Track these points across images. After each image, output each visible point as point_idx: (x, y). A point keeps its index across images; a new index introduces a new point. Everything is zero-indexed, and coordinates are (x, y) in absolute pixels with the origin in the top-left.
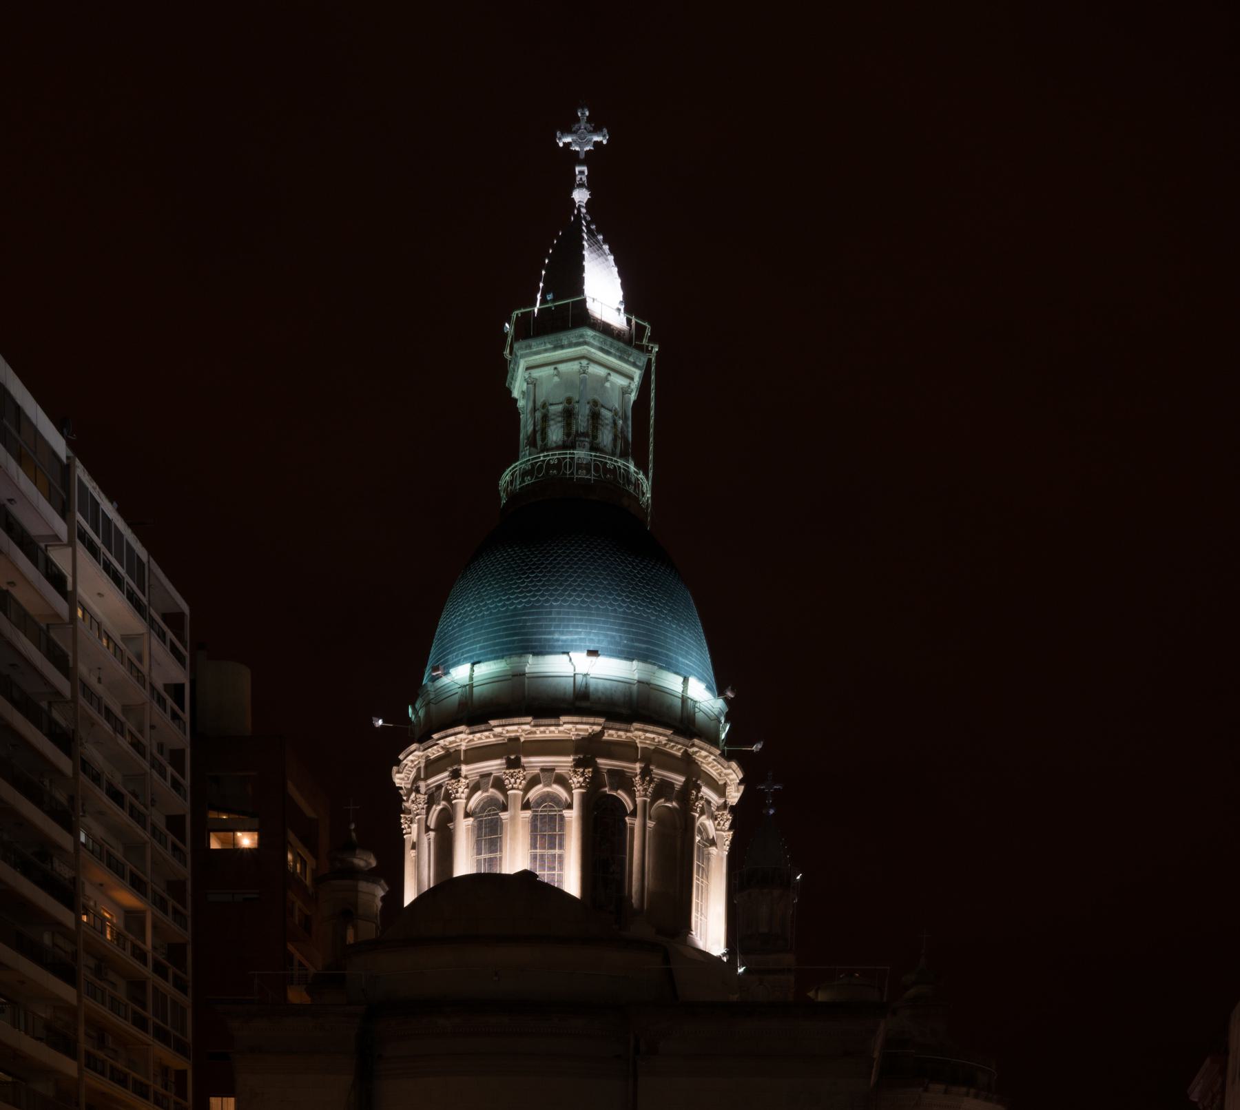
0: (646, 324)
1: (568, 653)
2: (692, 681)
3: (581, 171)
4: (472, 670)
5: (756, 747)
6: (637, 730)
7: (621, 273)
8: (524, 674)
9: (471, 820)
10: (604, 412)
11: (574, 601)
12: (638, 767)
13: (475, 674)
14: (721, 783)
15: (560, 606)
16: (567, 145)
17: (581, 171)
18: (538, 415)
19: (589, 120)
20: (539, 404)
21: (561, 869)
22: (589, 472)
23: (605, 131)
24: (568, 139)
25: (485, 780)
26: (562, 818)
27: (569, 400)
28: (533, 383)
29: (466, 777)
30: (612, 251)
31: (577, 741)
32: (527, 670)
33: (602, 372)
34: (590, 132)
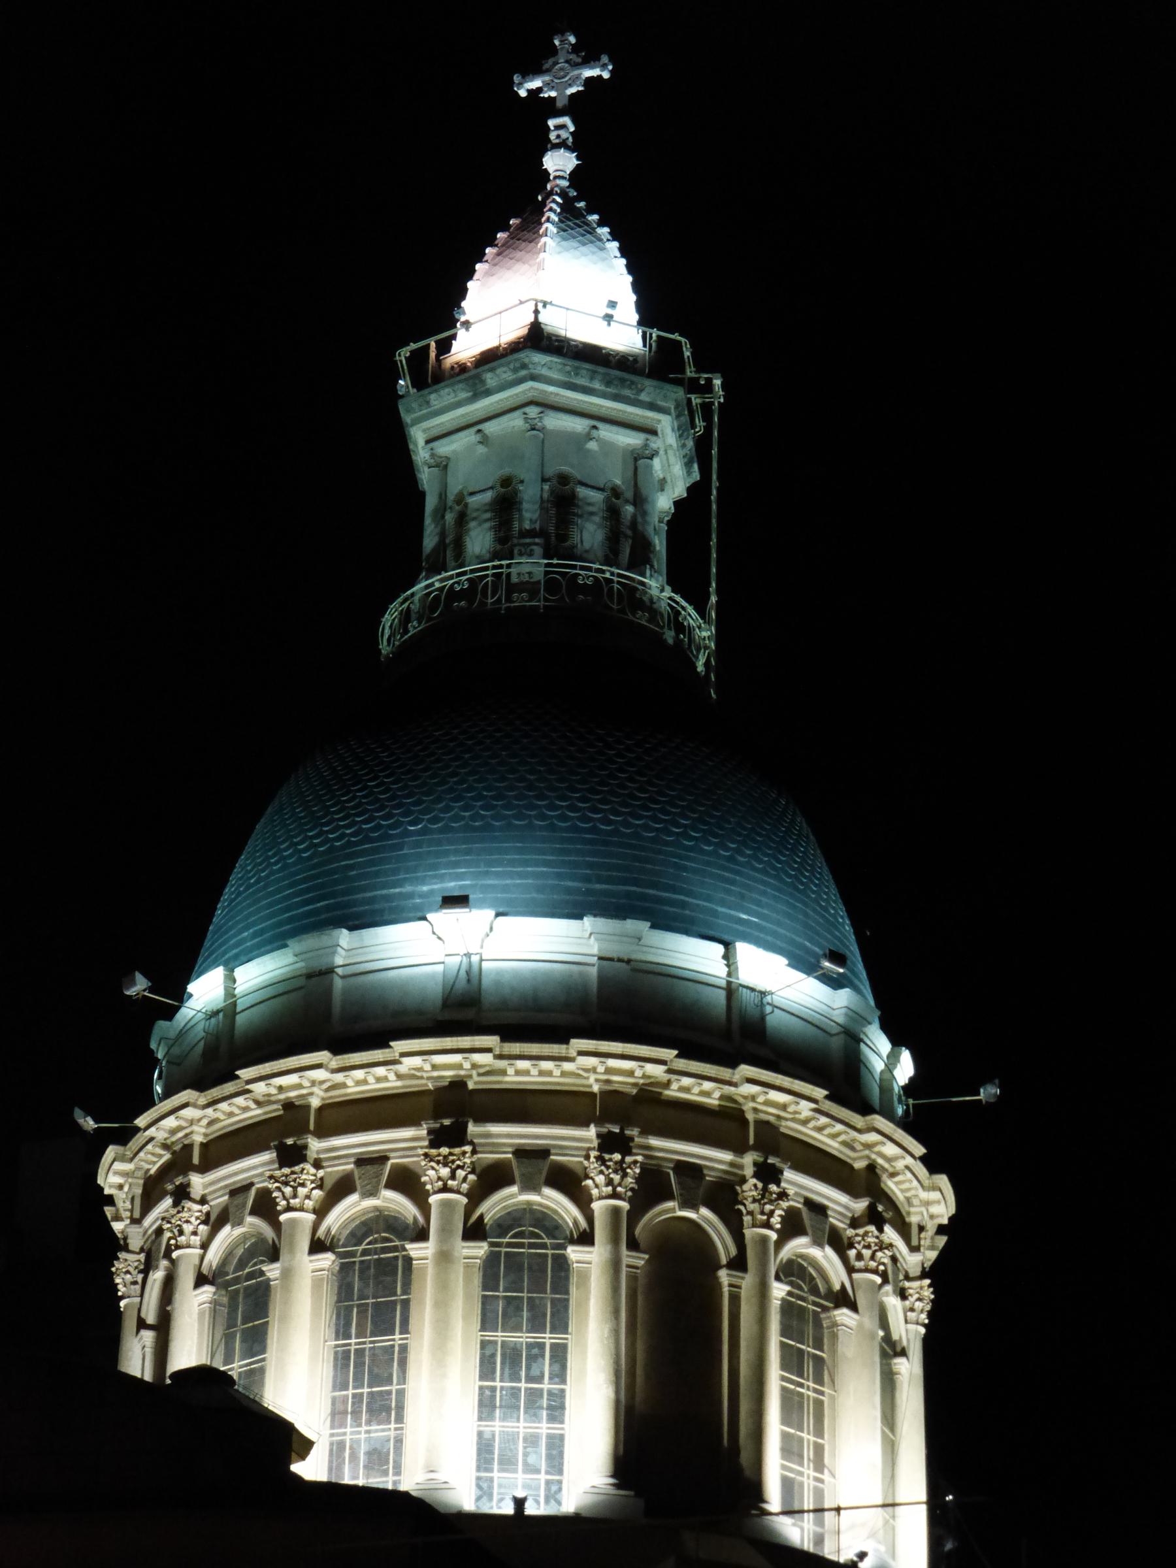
0: (676, 336)
1: (425, 919)
2: (743, 950)
3: (561, 126)
4: (230, 979)
5: (988, 1093)
6: (582, 1053)
7: (630, 269)
8: (330, 971)
9: (208, 1291)
10: (582, 492)
11: (456, 818)
12: (748, 1161)
13: (240, 989)
14: (859, 1165)
15: (423, 832)
16: (533, 93)
17: (561, 126)
18: (450, 517)
19: (575, 49)
20: (451, 497)
21: (403, 1379)
22: (534, 594)
23: (605, 59)
24: (536, 84)
25: (239, 1200)
26: (562, 1264)
27: (506, 482)
28: (442, 465)
29: (203, 1201)
30: (615, 236)
31: (439, 1090)
32: (339, 961)
33: (578, 425)
34: (576, 65)
